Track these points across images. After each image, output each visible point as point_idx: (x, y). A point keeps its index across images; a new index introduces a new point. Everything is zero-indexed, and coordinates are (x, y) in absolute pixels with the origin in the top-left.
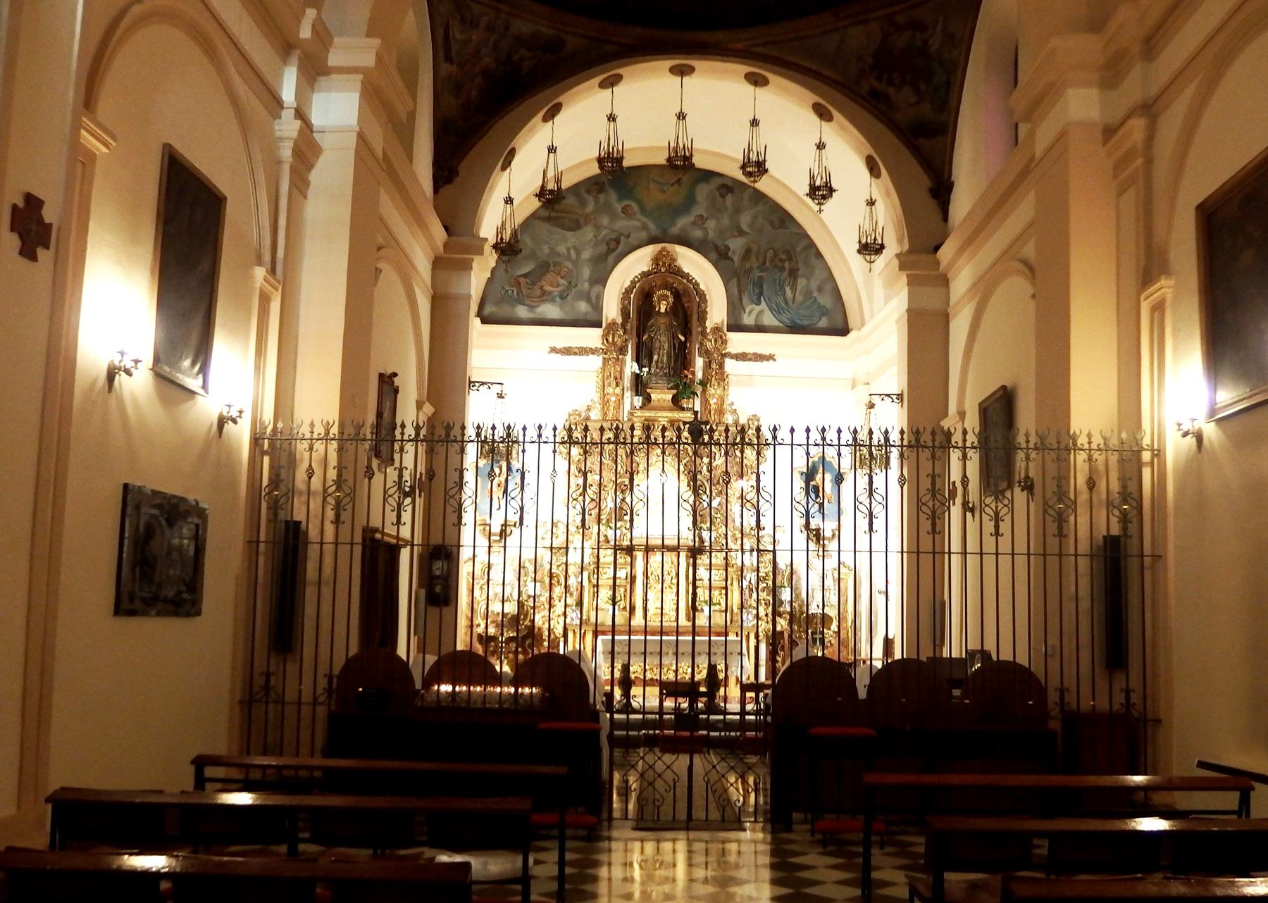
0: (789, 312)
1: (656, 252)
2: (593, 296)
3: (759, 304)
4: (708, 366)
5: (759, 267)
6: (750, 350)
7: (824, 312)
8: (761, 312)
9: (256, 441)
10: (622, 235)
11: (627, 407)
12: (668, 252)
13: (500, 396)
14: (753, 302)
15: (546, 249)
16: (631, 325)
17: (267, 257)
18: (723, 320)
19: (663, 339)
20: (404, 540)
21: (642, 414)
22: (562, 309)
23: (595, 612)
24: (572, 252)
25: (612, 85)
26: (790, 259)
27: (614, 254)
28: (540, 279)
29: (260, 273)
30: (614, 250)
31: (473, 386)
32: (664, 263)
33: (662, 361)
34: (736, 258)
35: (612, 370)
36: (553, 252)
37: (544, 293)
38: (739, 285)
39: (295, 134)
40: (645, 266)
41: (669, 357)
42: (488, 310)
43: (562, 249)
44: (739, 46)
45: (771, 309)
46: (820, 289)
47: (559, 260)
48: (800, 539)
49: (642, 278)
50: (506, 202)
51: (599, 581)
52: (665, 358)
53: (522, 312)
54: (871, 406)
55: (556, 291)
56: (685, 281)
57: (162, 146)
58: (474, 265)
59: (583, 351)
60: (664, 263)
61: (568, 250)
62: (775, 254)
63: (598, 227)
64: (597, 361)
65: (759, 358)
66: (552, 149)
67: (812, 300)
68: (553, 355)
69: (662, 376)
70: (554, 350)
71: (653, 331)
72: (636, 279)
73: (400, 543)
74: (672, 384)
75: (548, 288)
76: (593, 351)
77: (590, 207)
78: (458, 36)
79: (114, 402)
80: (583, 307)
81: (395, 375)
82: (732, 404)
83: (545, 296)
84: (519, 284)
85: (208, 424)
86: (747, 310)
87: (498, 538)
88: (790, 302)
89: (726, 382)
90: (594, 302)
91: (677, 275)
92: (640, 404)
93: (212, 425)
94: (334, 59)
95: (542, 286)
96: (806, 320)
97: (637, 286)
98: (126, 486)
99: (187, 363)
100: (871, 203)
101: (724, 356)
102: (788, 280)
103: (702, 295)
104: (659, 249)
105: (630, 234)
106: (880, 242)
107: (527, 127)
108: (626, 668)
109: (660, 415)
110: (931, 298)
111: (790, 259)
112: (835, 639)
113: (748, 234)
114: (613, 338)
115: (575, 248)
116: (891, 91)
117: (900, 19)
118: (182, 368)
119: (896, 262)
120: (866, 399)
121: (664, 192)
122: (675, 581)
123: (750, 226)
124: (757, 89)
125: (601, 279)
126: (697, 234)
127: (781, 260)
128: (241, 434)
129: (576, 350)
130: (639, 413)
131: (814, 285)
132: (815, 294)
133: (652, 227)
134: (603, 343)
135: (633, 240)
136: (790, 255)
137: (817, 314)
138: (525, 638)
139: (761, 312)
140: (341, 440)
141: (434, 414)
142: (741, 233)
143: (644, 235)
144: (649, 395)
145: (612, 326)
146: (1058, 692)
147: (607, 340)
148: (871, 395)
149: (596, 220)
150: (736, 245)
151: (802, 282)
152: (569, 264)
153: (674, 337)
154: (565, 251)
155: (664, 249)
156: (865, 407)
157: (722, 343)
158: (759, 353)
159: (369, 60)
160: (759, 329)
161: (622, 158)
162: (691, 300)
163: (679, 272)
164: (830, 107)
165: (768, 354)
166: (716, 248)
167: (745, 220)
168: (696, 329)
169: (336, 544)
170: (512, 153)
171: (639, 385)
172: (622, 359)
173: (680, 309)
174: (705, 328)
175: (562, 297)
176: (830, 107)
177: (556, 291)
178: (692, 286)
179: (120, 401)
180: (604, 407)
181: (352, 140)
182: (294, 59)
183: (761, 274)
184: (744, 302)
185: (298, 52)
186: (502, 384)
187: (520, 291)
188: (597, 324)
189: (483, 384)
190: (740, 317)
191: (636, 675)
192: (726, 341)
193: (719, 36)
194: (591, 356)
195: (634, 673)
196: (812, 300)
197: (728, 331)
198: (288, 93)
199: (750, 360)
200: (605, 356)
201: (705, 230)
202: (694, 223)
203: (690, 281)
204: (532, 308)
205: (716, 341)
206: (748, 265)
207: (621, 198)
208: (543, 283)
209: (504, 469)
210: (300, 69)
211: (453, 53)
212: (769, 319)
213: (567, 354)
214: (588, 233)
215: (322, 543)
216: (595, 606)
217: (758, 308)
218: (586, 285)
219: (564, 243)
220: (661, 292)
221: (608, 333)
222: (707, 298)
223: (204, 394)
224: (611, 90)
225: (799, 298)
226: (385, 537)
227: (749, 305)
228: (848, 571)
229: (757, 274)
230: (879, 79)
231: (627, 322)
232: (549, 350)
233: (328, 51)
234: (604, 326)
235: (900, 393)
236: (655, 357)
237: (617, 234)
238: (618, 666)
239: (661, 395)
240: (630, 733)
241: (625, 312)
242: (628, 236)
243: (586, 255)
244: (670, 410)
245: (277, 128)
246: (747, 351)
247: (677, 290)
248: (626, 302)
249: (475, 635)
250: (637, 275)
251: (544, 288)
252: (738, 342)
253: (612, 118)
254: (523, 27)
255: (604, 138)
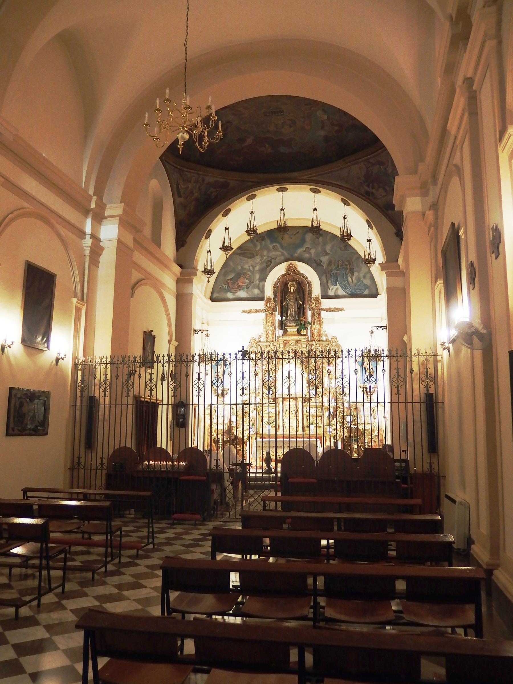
0: (350, 288)
1: (287, 266)
2: (261, 286)
3: (336, 286)
4: (313, 315)
5: (335, 269)
6: (332, 306)
7: (366, 287)
8: (337, 289)
9: (75, 365)
10: (272, 258)
11: (277, 335)
12: (293, 265)
13: (207, 336)
14: (333, 285)
15: (239, 267)
16: (278, 298)
17: (79, 293)
18: (319, 295)
19: (292, 304)
20: (159, 400)
21: (283, 338)
22: (247, 293)
23: (262, 428)
24: (251, 268)
25: (252, 199)
26: (350, 264)
27: (270, 267)
28: (237, 281)
29: (75, 300)
30: (269, 266)
31: (196, 332)
32: (291, 270)
33: (292, 314)
34: (325, 266)
35: (270, 319)
36: (243, 268)
37: (239, 286)
38: (326, 277)
39: (90, 245)
40: (284, 272)
41: (295, 312)
42: (215, 295)
43: (246, 267)
44: (305, 177)
45: (342, 287)
46: (364, 277)
47: (245, 271)
48: (360, 391)
49: (282, 277)
50: (314, 211)
51: (263, 414)
52: (293, 312)
53: (230, 295)
54: (372, 332)
55: (244, 285)
56: (301, 277)
57: (25, 262)
58: (194, 280)
59: (257, 311)
60: (291, 270)
61: (249, 266)
62: (343, 262)
63: (262, 256)
64: (263, 315)
65: (337, 310)
66: (227, 229)
67: (361, 282)
68: (244, 313)
69: (292, 320)
70: (244, 311)
71: (288, 300)
72: (280, 278)
73: (158, 402)
74: (296, 324)
75: (240, 284)
76: (261, 311)
77: (258, 248)
78: (183, 186)
79: (5, 358)
80: (256, 291)
81: (152, 331)
82: (325, 331)
83: (240, 288)
84: (228, 283)
85: (51, 361)
86: (331, 288)
87: (221, 396)
88: (351, 284)
89: (322, 322)
90: (261, 289)
91: (298, 275)
92: (282, 334)
93: (52, 362)
94: (107, 213)
95: (238, 284)
96: (359, 291)
97: (280, 281)
98: (11, 389)
99: (39, 339)
100: (369, 241)
101: (320, 310)
102: (349, 273)
103: (310, 283)
104: (289, 264)
105: (276, 258)
106: (374, 258)
107: (216, 220)
108: (268, 454)
109: (291, 338)
110: (398, 282)
111: (350, 264)
112: (377, 439)
113: (330, 254)
114: (269, 305)
115: (252, 265)
116: (374, 191)
117: (372, 161)
118: (37, 341)
119: (380, 267)
120: (371, 329)
121: (291, 238)
122: (284, 414)
123: (331, 251)
124: (316, 194)
125: (263, 279)
126: (307, 255)
127: (346, 265)
128: (67, 364)
129: (254, 311)
130: (281, 338)
131: (362, 275)
132: (362, 279)
133: (286, 254)
134: (265, 307)
135: (278, 260)
136: (350, 262)
137: (363, 288)
138: (233, 440)
139: (337, 289)
140: (111, 363)
141: (178, 345)
142: (327, 254)
143: (282, 258)
144: (286, 329)
145: (269, 299)
146: (429, 464)
147: (267, 306)
148: (372, 327)
149: (261, 253)
150: (324, 259)
151: (356, 274)
152: (250, 273)
153: (297, 303)
154: (248, 267)
155: (291, 264)
156: (370, 333)
157: (319, 304)
158: (337, 307)
159: (120, 212)
160: (337, 297)
161: (257, 229)
162: (305, 285)
163: (299, 273)
164: (349, 201)
165: (341, 308)
166: (316, 262)
167: (328, 248)
168: (307, 298)
169: (110, 405)
170: (210, 232)
171: (282, 326)
172: (274, 314)
173: (301, 289)
174: (311, 298)
175: (247, 288)
176: (349, 201)
177: (244, 285)
178: (305, 279)
179: (8, 358)
180: (267, 335)
181: (115, 243)
182: (90, 216)
183: (337, 272)
184: (329, 285)
185: (91, 212)
186: (208, 330)
187: (228, 286)
188: (262, 299)
189: (200, 330)
190: (327, 292)
191: (280, 457)
192: (321, 303)
193: (296, 174)
194: (261, 313)
195: (279, 456)
196: (361, 282)
197: (321, 298)
198: (88, 229)
199: (333, 311)
200: (267, 313)
201: (310, 254)
202: (305, 251)
203: (304, 277)
204: (234, 293)
205: (316, 303)
206: (330, 268)
207: (272, 242)
208: (239, 282)
209: (223, 365)
210: (93, 219)
211: (182, 193)
212: (341, 292)
213: (250, 313)
214: (258, 259)
215: (105, 405)
216: (262, 426)
217: (335, 287)
218: (257, 282)
219: (248, 264)
220: (291, 283)
221: (267, 302)
222: (312, 284)
223: (48, 350)
224: (251, 201)
225: (355, 281)
226: (146, 400)
227: (331, 287)
228: (382, 407)
229: (334, 272)
230: (368, 186)
231: (276, 297)
232: (242, 311)
233: (105, 210)
234: (265, 300)
235: (386, 325)
236: (289, 312)
237: (271, 258)
238: (265, 453)
239: (292, 329)
240: (265, 483)
241: (275, 293)
242: (275, 259)
243: (257, 268)
244: (295, 336)
245: (83, 243)
246: (331, 307)
247: (299, 282)
248: (275, 288)
249: (212, 440)
250: (280, 276)
251: (239, 284)
252: (326, 303)
253: (252, 213)
254: (210, 179)
255: (248, 222)
